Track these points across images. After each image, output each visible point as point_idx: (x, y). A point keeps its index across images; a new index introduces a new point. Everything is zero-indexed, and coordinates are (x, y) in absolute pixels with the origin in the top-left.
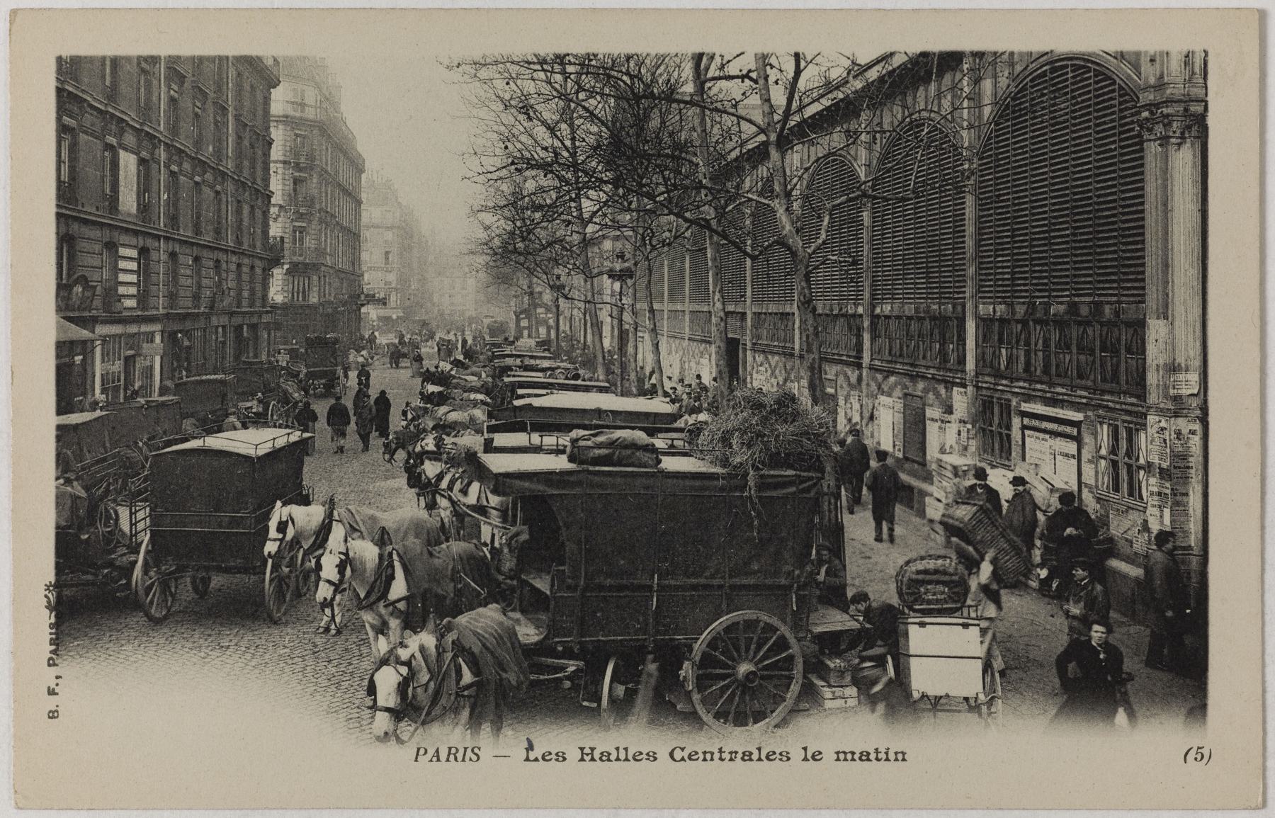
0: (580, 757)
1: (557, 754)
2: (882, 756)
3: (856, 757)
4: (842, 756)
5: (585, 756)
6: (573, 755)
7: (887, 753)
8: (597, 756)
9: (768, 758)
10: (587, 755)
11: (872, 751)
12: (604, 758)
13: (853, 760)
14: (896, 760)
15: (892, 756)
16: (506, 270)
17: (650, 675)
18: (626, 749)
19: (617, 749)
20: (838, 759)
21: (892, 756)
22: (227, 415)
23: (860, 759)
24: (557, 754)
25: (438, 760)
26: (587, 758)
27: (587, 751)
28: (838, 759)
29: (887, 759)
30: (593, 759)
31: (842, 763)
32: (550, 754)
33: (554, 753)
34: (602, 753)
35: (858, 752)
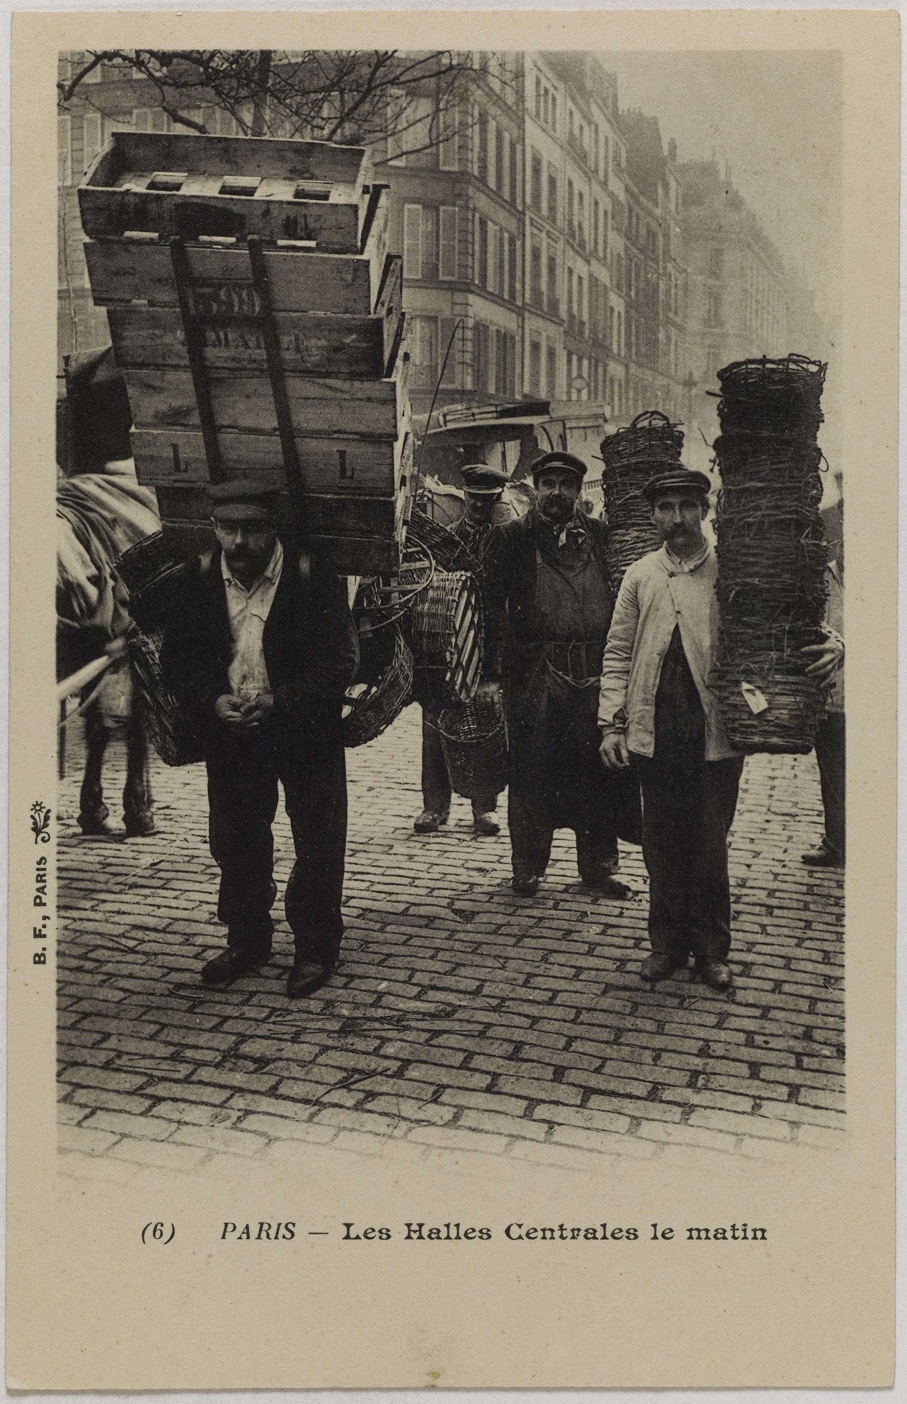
1: (628, 1232)
3: (711, 1234)
5: (412, 1234)
7: (745, 1230)
8: (425, 1232)
9: (663, 1235)
10: (415, 1232)
12: (589, 1236)
13: (707, 1238)
14: (755, 1238)
15: (750, 1234)
19: (448, 1226)
20: (691, 1238)
21: (750, 1234)
25: (248, 1237)
27: (415, 1227)
28: (691, 1238)
29: (745, 1238)
30: (421, 1237)
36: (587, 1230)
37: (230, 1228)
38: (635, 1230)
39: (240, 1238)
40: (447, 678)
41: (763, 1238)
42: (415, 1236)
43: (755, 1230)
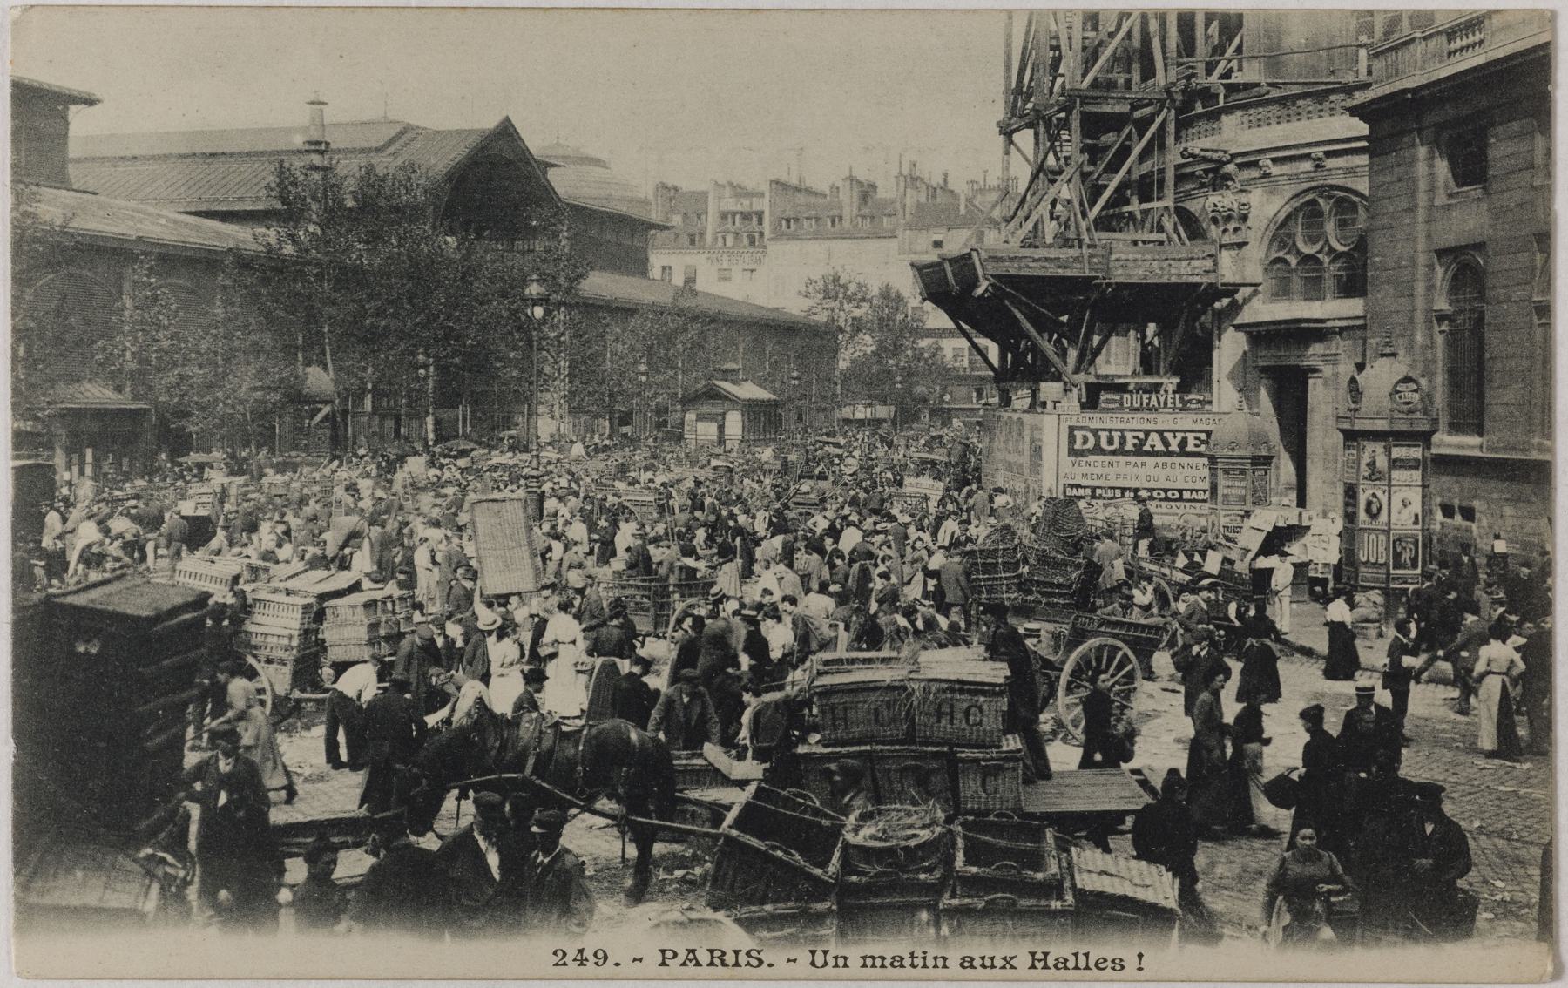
1: (1113, 961)
2: (987, 963)
3: (887, 963)
4: (869, 962)
5: (1037, 963)
6: (1023, 960)
7: (924, 958)
9: (1097, 965)
10: (1040, 961)
13: (883, 966)
15: (930, 962)
17: (933, 832)
18: (1087, 955)
19: (1076, 955)
20: (865, 966)
21: (930, 962)
22: (351, 210)
24: (1113, 961)
26: (1039, 965)
28: (865, 966)
29: (925, 966)
30: (1046, 967)
33: (1109, 960)
39: (684, 964)
40: (1010, 356)
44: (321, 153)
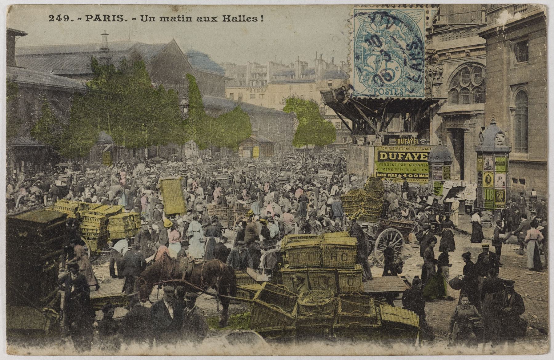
0: (223, 19)
1: (253, 18)
7: (183, 18)
8: (231, 19)
9: (247, 20)
10: (227, 19)
11: (176, 17)
12: (234, 20)
14: (187, 21)
15: (185, 19)
16: (526, 334)
19: (240, 16)
20: (161, 21)
21: (185, 19)
23: (171, 20)
27: (227, 17)
28: (161, 21)
29: (183, 21)
30: (229, 21)
31: (227, 22)
32: (250, 18)
34: (233, 18)
35: (170, 17)
36: (172, 18)
37: (90, 17)
38: (256, 18)
41: (191, 21)
42: (227, 20)
43: (187, 18)
44: (106, 52)
